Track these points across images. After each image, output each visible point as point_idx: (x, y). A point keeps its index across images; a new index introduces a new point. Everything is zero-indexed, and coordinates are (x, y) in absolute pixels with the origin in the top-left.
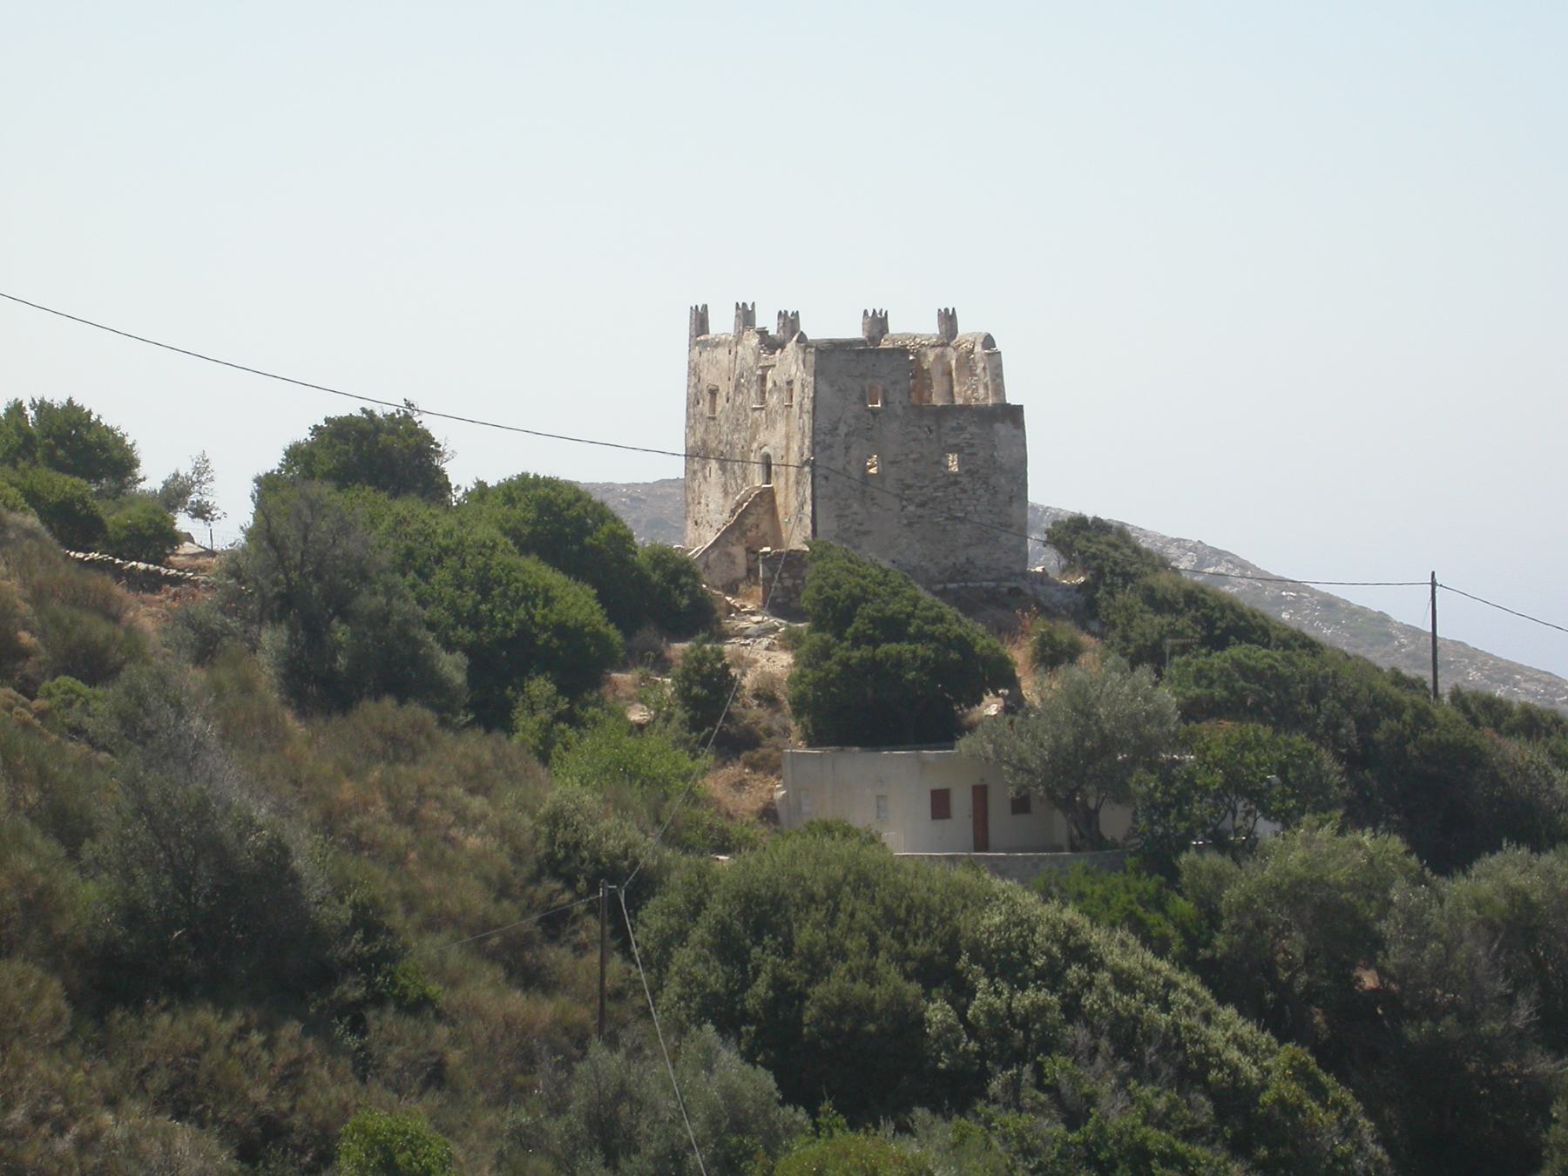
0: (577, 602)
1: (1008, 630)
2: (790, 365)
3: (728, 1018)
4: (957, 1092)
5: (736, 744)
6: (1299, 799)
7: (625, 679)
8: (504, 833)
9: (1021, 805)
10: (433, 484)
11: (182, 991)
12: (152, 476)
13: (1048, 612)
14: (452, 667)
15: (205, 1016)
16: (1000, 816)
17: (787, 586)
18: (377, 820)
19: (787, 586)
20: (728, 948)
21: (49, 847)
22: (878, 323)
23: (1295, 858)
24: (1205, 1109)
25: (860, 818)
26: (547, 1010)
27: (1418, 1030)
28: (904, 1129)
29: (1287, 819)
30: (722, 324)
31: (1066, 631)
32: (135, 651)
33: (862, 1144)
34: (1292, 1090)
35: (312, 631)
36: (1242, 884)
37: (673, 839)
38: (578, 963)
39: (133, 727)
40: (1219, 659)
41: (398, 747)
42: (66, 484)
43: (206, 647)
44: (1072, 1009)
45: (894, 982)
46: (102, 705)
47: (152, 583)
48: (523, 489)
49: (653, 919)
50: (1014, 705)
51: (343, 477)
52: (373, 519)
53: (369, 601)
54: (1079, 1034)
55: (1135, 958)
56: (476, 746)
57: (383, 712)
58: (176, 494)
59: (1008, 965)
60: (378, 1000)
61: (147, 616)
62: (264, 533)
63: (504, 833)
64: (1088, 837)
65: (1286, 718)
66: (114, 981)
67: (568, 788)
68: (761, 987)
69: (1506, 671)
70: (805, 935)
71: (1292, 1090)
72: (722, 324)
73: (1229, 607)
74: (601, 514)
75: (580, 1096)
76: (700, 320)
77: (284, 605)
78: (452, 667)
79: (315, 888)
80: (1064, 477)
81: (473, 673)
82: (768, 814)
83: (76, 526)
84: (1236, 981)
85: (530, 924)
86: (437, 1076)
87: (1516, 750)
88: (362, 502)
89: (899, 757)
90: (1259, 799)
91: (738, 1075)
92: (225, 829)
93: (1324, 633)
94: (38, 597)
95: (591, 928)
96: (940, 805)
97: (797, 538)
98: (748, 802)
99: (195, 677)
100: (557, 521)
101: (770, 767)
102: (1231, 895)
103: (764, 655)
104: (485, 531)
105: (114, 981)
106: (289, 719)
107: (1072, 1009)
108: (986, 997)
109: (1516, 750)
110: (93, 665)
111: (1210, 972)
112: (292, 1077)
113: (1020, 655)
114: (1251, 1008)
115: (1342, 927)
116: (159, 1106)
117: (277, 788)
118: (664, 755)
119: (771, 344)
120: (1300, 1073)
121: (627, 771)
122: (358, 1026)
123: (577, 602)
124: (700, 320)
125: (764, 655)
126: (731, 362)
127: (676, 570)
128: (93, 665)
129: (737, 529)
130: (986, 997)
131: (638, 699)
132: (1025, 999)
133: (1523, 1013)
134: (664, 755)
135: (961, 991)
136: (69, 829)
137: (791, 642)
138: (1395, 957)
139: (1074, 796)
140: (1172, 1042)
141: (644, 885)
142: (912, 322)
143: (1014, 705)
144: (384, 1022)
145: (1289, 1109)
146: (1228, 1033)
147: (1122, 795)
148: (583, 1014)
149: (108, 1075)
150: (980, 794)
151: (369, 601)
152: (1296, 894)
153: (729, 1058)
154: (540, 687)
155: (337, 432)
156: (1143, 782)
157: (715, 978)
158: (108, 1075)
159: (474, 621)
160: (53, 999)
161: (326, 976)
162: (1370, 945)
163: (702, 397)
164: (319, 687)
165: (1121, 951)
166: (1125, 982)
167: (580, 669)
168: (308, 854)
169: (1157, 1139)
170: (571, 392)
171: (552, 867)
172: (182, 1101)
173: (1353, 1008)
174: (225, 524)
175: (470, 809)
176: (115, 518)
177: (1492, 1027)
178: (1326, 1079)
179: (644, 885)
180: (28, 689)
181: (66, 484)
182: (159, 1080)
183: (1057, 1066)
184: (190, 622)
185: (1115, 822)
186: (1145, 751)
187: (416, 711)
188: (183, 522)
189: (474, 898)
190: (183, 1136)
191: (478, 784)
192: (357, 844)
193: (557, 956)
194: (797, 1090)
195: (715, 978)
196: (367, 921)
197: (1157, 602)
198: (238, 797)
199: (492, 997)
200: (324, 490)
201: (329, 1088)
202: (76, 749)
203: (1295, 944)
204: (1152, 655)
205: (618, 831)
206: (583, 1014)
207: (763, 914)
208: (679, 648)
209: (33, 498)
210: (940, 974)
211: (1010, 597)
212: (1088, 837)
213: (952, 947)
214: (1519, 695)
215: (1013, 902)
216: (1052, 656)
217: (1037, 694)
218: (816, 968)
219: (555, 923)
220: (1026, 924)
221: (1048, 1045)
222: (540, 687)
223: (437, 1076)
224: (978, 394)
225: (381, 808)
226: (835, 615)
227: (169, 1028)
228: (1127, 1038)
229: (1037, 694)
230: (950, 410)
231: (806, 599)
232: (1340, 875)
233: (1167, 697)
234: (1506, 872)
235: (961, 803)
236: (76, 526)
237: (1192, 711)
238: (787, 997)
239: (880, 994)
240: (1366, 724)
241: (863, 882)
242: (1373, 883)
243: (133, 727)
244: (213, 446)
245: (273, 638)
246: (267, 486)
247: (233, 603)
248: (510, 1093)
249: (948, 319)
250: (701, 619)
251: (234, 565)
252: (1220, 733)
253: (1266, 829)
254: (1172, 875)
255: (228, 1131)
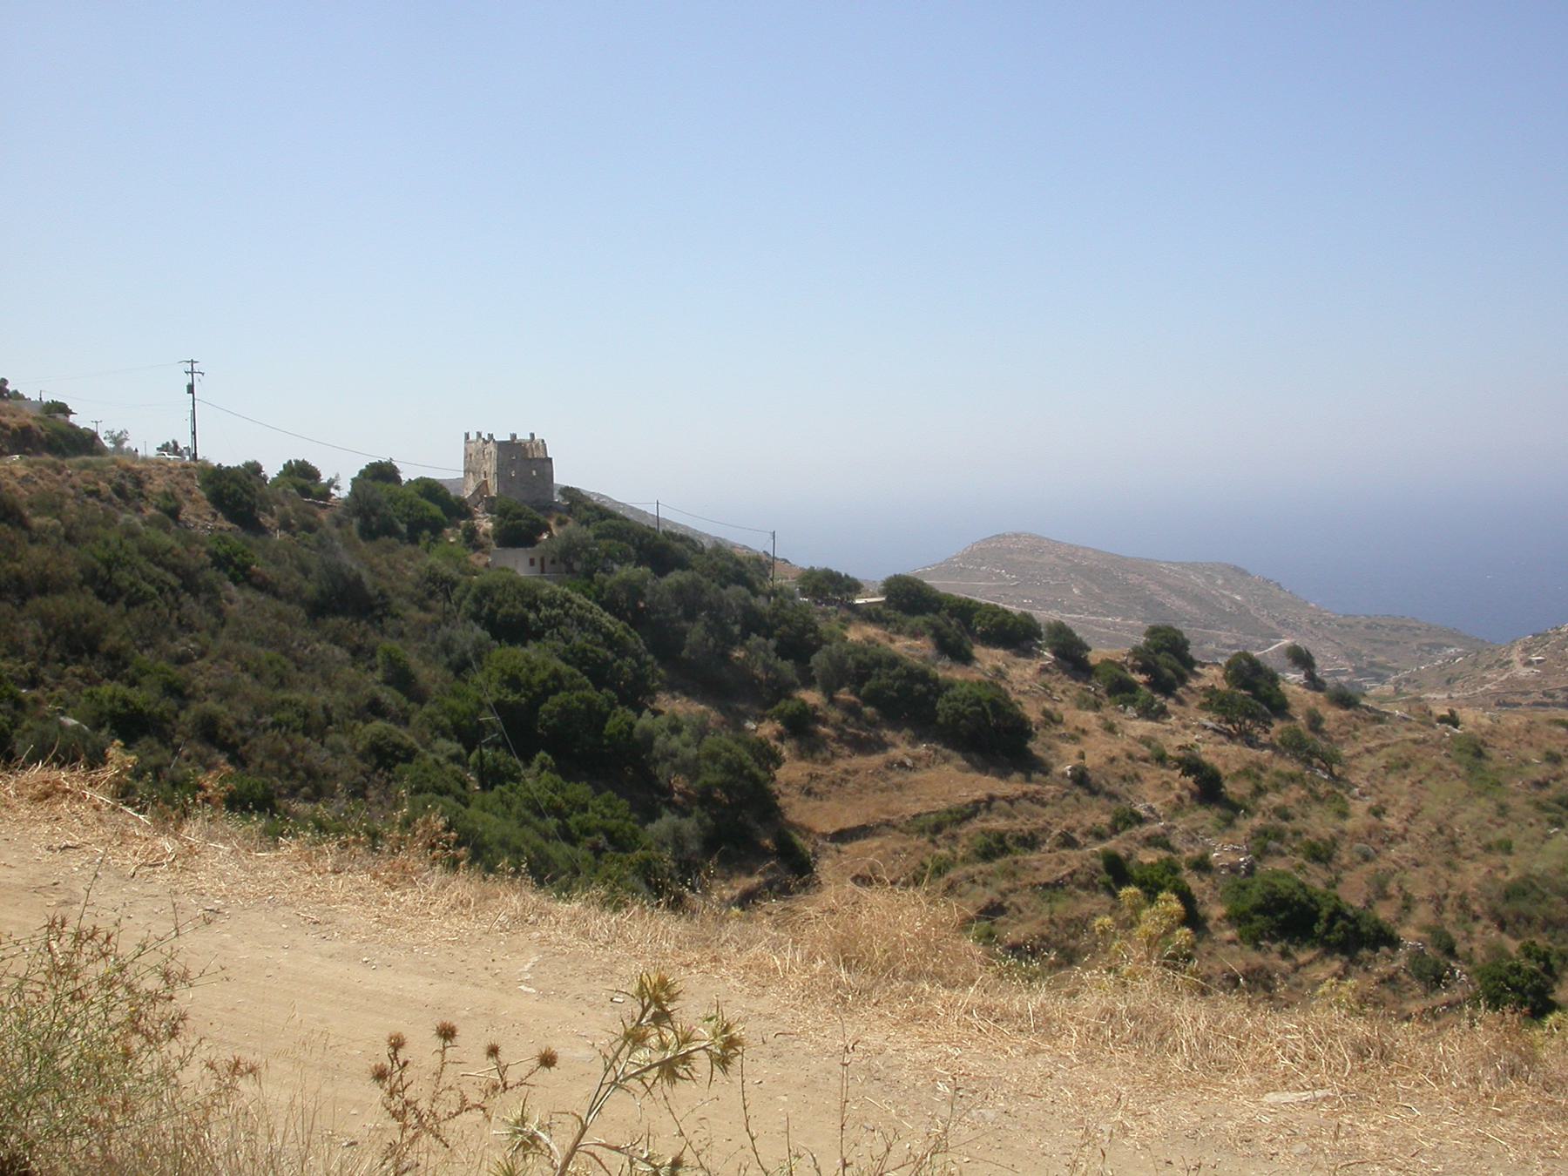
0: (436, 510)
1: (549, 516)
2: (491, 448)
3: (476, 617)
4: (538, 636)
5: (478, 547)
6: (624, 559)
7: (448, 530)
8: (417, 571)
9: (553, 562)
10: (398, 480)
11: (335, 613)
12: (324, 479)
13: (560, 511)
14: (403, 528)
15: (341, 619)
16: (547, 563)
17: (491, 506)
18: (384, 567)
19: (491, 506)
20: (477, 601)
21: (300, 575)
22: (514, 436)
23: (624, 574)
24: (601, 638)
25: (511, 566)
26: (429, 617)
27: (481, 757)
28: (525, 645)
29: (621, 564)
30: (473, 437)
31: (564, 516)
32: (321, 524)
33: (512, 650)
34: (623, 633)
35: (366, 519)
36: (610, 581)
37: (462, 572)
38: (438, 605)
39: (321, 545)
40: (604, 523)
41: (389, 549)
42: (303, 481)
43: (339, 523)
44: (566, 614)
45: (520, 608)
46: (312, 538)
47: (325, 507)
48: (421, 481)
49: (457, 593)
50: (551, 536)
51: (374, 478)
52: (382, 489)
53: (381, 511)
54: (568, 620)
55: (583, 601)
56: (409, 548)
57: (385, 540)
58: (331, 483)
59: (550, 603)
60: (386, 614)
61: (324, 516)
62: (353, 493)
63: (417, 571)
64: (570, 570)
65: (621, 538)
66: (318, 610)
67: (434, 559)
68: (486, 610)
69: (676, 525)
70: (497, 597)
71: (623, 633)
72: (473, 437)
73: (606, 509)
74: (442, 487)
75: (439, 639)
76: (467, 436)
77: (358, 512)
78: (403, 528)
79: (369, 586)
80: (562, 477)
81: (409, 529)
82: (487, 565)
83: (304, 492)
84: (607, 606)
85: (425, 595)
86: (401, 634)
87: (678, 545)
88: (379, 485)
89: (520, 550)
90: (614, 559)
91: (480, 633)
92: (345, 571)
93: (631, 516)
94: (296, 511)
95: (441, 596)
96: (532, 562)
97: (493, 493)
98: (481, 562)
99: (336, 531)
100: (430, 489)
101: (488, 553)
102: (607, 584)
103: (485, 524)
104: (411, 492)
105: (318, 610)
106: (361, 542)
107: (566, 614)
108: (544, 612)
109: (678, 545)
110: (310, 528)
111: (602, 604)
112: (364, 635)
113: (552, 523)
114: (613, 613)
115: (635, 591)
116: (331, 641)
117: (358, 560)
118: (459, 550)
119: (486, 442)
120: (625, 629)
121: (451, 555)
122: (381, 621)
123: (436, 510)
124: (467, 436)
125: (485, 524)
126: (475, 447)
127: (462, 502)
128: (310, 528)
129: (477, 491)
130: (544, 612)
131: (452, 536)
132: (554, 612)
133: (680, 612)
134: (459, 550)
135: (538, 610)
136: (305, 571)
137: (492, 520)
138: (648, 599)
139: (567, 559)
140: (593, 622)
141: (455, 584)
142: (523, 436)
143: (551, 536)
144: (388, 621)
145: (622, 638)
146: (607, 619)
147: (579, 559)
148: (439, 618)
149: (317, 634)
150: (542, 560)
151: (381, 511)
152: (626, 584)
153: (478, 629)
154: (426, 533)
155: (372, 467)
156: (584, 555)
157: (473, 608)
158: (317, 634)
159: (408, 515)
160: (302, 614)
161: (372, 608)
162: (642, 595)
163: (468, 456)
164: (368, 533)
165: (578, 598)
166: (580, 607)
167: (436, 528)
168: (367, 577)
169: (589, 646)
170: (433, 456)
171: (429, 579)
172: (336, 640)
173: (638, 612)
174: (343, 491)
175: (409, 565)
176: (315, 490)
177: (672, 615)
178: (604, 652)
179: (455, 584)
180: (294, 534)
181: (303, 481)
182: (330, 635)
183: (562, 629)
184: (335, 517)
185: (577, 566)
186: (585, 547)
187: (394, 540)
188: (333, 491)
189: (409, 587)
190: (337, 650)
191: (410, 559)
192: (379, 574)
193: (432, 603)
194: (496, 636)
195: (473, 608)
196: (382, 594)
197: (588, 509)
198: (348, 562)
199: (415, 614)
200: (369, 482)
201: (373, 638)
202: (305, 550)
203: (623, 596)
204: (587, 522)
205: (447, 570)
206: (439, 618)
207: (485, 591)
208: (463, 522)
209: (294, 485)
210: (532, 606)
211: (548, 508)
212: (570, 570)
213: (535, 599)
214: (680, 532)
215: (551, 587)
216: (561, 523)
217: (556, 533)
218: (500, 605)
219: (431, 594)
220: (555, 593)
221: (561, 623)
222: (426, 533)
223: (401, 634)
224: (542, 455)
225: (385, 565)
226: (503, 513)
227: (332, 622)
228: (581, 621)
229: (556, 533)
230: (534, 459)
231: (496, 508)
232: (635, 578)
233: (591, 533)
234: (675, 577)
235: (538, 562)
236: (304, 492)
237: (597, 537)
238: (492, 612)
239: (517, 612)
240: (641, 540)
241: (512, 583)
242: (643, 580)
243: (321, 545)
244: (340, 472)
245: (356, 521)
246: (354, 480)
247: (346, 512)
248: (420, 639)
249: (532, 435)
250: (468, 514)
251: (346, 502)
252: (604, 543)
253: (616, 567)
254: (592, 579)
255: (348, 648)
